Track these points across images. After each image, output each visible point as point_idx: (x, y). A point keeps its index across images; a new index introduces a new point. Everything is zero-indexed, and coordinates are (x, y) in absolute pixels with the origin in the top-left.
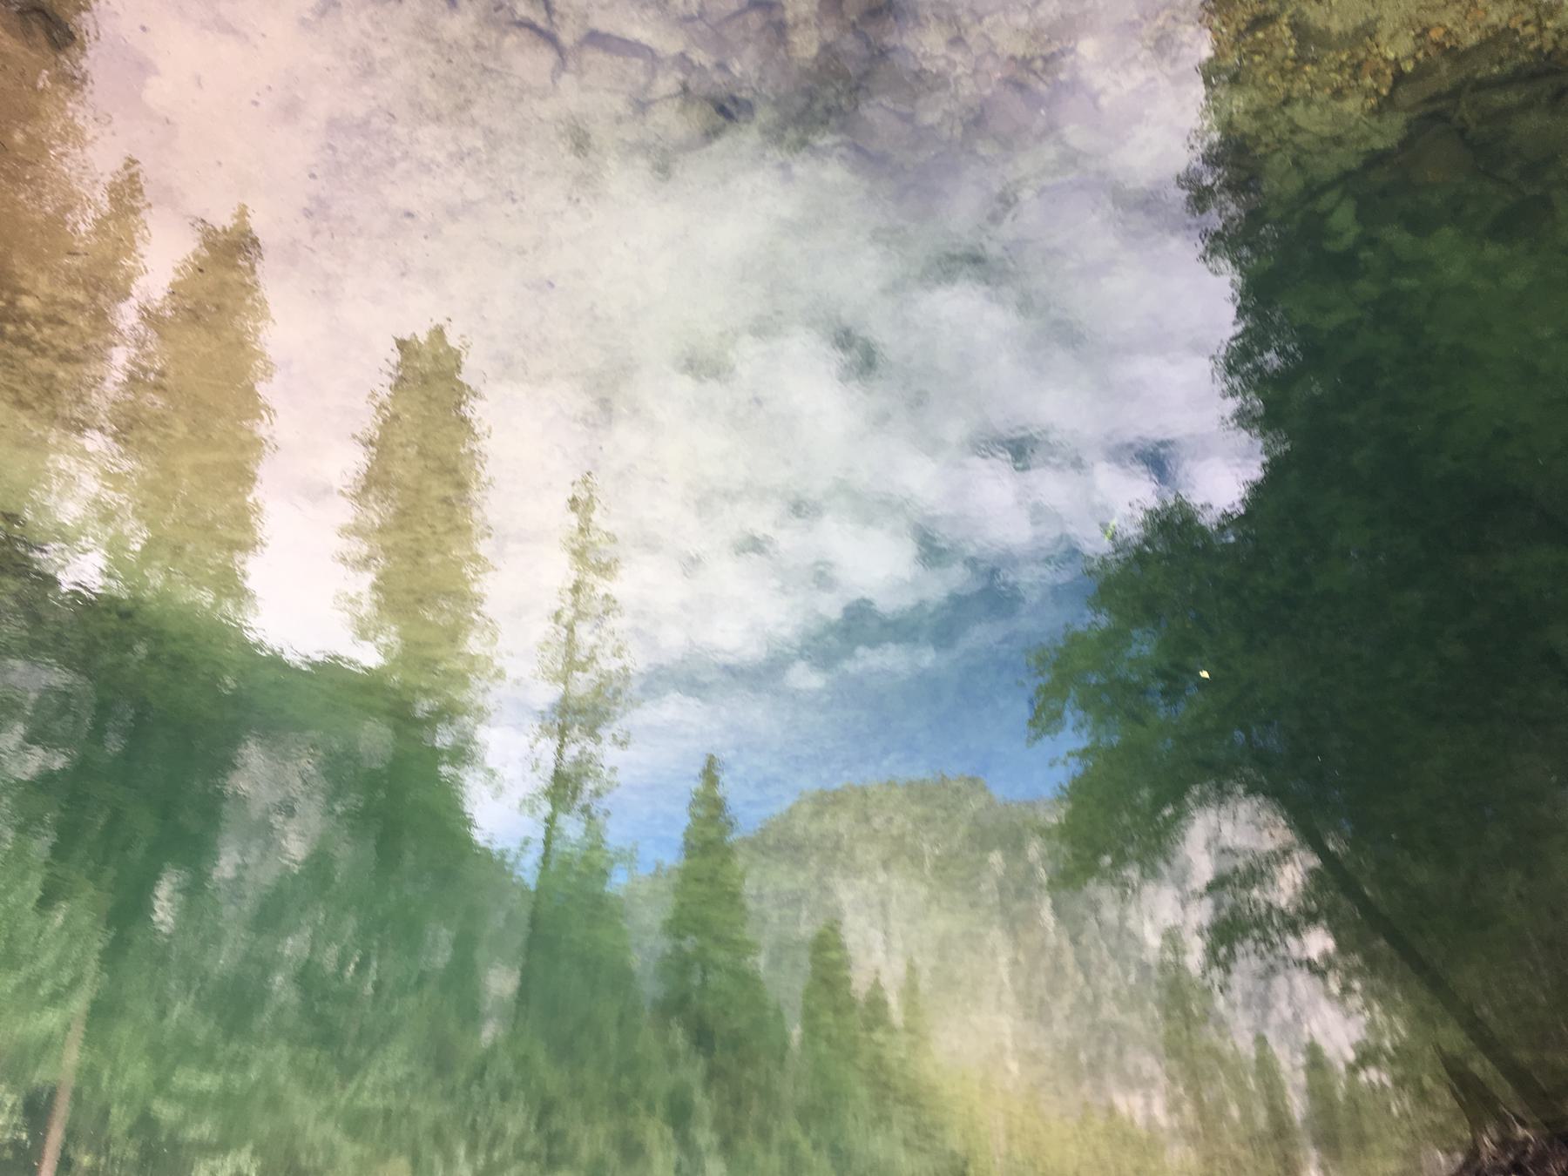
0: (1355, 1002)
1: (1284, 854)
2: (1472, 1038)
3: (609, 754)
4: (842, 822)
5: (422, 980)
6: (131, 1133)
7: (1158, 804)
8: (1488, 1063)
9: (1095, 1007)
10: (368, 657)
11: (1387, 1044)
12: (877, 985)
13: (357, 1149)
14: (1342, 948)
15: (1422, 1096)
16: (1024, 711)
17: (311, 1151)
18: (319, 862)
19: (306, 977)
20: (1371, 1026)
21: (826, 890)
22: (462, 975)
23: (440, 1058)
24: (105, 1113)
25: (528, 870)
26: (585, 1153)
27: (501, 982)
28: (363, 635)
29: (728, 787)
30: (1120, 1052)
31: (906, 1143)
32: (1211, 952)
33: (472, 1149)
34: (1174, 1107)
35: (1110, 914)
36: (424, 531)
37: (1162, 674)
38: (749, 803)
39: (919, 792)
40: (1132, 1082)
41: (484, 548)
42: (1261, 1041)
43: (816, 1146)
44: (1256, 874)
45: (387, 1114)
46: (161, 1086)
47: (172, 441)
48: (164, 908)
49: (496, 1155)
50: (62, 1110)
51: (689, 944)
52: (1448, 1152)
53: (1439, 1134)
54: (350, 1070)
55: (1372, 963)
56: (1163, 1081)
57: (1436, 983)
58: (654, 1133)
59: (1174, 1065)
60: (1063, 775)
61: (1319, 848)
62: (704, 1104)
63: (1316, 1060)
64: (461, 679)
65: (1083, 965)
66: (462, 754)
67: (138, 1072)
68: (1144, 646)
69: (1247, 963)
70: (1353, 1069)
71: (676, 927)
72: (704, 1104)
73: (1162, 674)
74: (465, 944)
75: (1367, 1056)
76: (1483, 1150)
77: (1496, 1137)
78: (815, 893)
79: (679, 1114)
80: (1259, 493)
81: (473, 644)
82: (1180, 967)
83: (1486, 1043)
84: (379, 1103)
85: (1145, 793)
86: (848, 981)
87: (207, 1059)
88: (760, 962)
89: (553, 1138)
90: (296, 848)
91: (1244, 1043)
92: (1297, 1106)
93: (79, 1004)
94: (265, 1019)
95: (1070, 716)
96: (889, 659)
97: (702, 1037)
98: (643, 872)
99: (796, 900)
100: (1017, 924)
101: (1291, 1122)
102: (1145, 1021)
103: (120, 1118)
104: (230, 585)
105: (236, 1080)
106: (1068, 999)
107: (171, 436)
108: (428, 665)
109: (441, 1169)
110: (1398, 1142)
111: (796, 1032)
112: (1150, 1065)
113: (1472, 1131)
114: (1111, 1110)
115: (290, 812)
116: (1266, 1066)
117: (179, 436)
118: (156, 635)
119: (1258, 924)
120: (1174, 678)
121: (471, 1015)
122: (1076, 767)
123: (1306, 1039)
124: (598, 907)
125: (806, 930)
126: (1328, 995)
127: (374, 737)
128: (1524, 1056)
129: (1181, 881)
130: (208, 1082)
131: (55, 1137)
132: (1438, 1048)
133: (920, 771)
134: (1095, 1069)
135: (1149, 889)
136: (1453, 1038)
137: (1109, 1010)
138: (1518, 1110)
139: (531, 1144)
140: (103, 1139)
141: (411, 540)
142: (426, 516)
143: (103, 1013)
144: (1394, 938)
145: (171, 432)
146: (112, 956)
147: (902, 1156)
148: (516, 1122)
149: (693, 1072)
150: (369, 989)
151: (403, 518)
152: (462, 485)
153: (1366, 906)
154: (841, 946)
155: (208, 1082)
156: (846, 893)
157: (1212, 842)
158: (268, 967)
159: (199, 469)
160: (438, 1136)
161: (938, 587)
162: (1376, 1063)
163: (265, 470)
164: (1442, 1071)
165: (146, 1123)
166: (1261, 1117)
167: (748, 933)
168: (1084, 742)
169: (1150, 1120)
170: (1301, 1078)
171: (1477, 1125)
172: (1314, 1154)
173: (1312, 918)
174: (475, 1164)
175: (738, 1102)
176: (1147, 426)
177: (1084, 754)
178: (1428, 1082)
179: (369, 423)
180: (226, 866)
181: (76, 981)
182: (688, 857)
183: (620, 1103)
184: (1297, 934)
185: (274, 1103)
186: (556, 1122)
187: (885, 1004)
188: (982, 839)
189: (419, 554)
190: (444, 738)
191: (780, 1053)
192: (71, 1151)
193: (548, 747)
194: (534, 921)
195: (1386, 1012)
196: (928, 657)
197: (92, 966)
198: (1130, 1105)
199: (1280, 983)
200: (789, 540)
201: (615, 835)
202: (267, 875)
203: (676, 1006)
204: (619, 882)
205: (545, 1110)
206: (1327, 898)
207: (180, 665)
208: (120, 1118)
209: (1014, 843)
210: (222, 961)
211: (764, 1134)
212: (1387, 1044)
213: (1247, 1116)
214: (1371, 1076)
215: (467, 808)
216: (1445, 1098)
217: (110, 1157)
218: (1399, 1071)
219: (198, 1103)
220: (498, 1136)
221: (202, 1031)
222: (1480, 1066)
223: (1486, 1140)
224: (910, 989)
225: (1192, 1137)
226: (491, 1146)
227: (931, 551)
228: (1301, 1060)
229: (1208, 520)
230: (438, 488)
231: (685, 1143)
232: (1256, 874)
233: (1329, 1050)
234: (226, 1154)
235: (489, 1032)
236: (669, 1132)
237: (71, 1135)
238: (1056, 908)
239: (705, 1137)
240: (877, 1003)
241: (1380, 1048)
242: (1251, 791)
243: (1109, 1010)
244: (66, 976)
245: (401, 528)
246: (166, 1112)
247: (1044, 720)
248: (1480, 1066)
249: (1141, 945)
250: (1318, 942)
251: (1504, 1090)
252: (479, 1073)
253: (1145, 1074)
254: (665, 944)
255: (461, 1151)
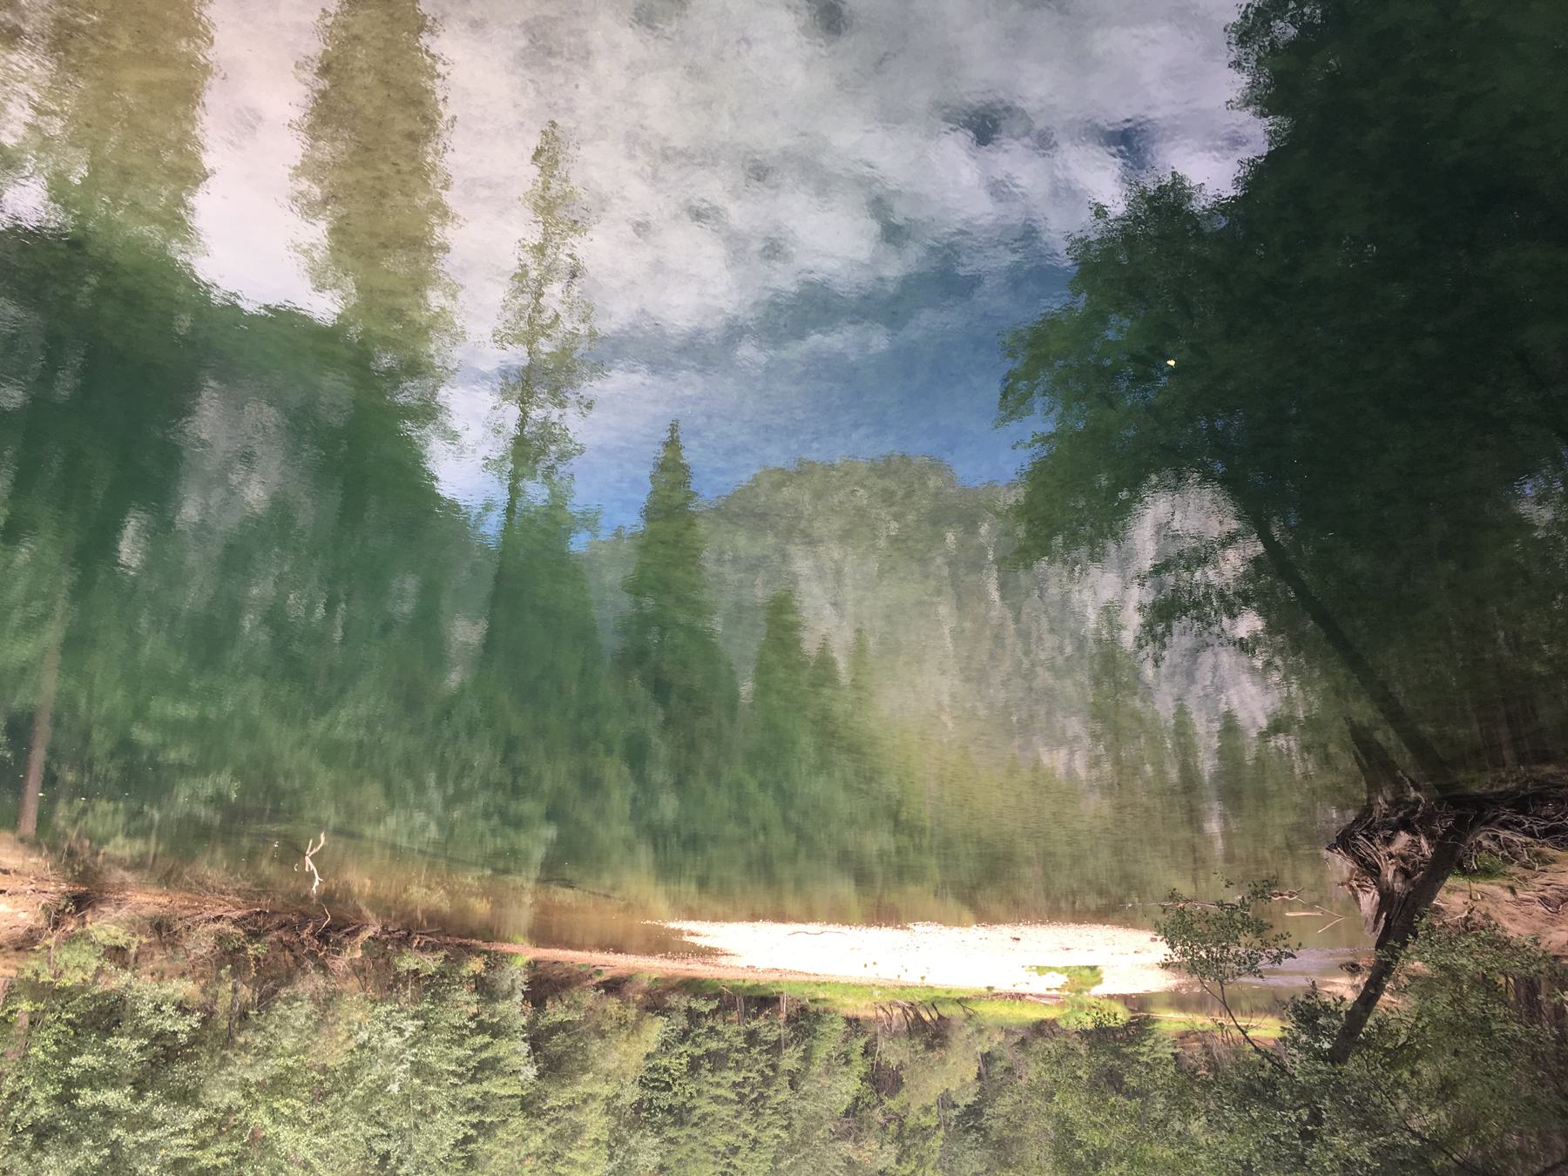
0: (1276, 677)
1: (1230, 540)
2: (1382, 711)
3: (572, 422)
4: (797, 495)
5: (387, 628)
6: (112, 755)
7: (1116, 489)
8: (1392, 733)
9: (1029, 675)
10: (324, 307)
11: (1301, 714)
12: (824, 648)
13: (331, 776)
14: (1271, 629)
15: (1327, 761)
16: (996, 390)
17: (288, 775)
18: (281, 508)
19: (274, 618)
20: (1288, 700)
21: (785, 557)
22: (427, 624)
23: (411, 698)
24: (86, 737)
25: (492, 525)
26: (546, 786)
27: (465, 632)
28: (320, 288)
29: (691, 454)
30: (1049, 713)
31: (847, 787)
32: (1148, 627)
33: (441, 780)
34: (1095, 763)
35: (1054, 591)
36: (386, 169)
37: (1135, 358)
38: (717, 471)
39: (884, 468)
40: (1058, 740)
41: (450, 198)
42: (1181, 711)
43: (763, 786)
44: (1201, 557)
45: (360, 744)
46: (139, 713)
47: (116, 53)
48: (130, 550)
49: (466, 784)
50: (43, 734)
51: (649, 602)
52: (1342, 809)
53: (1337, 794)
54: (323, 707)
55: (1297, 645)
56: (1087, 741)
57: (1354, 660)
58: (613, 770)
59: (1098, 727)
60: (1024, 458)
61: (1266, 538)
62: (661, 748)
63: (1230, 727)
64: (422, 332)
65: (1024, 635)
66: (428, 412)
67: (116, 699)
68: (1119, 329)
69: (1182, 637)
70: (1264, 736)
71: (636, 588)
72: (661, 748)
73: (1135, 358)
74: (430, 594)
75: (1278, 726)
76: (1377, 808)
77: (1389, 798)
78: (776, 558)
79: (636, 755)
80: (1259, 177)
81: (436, 299)
82: (1114, 641)
83: (1395, 715)
84: (353, 736)
85: (1103, 481)
86: (798, 641)
87: (181, 691)
88: (717, 624)
89: (516, 771)
90: (255, 495)
91: (1164, 707)
92: (1207, 765)
93: (53, 634)
94: (235, 656)
95: (1039, 402)
96: (835, 341)
97: (661, 689)
98: (605, 535)
99: (754, 566)
100: (964, 598)
101: (1199, 776)
102: (1077, 687)
103: (101, 741)
104: (176, 223)
105: (212, 712)
106: (1007, 666)
107: (114, 48)
108: (396, 314)
109: (412, 795)
110: (1297, 798)
111: (746, 688)
112: (1075, 726)
113: (1369, 792)
114: (1036, 766)
115: (247, 458)
116: (1182, 728)
117: (122, 47)
118: (106, 268)
119: (1197, 605)
120: (1145, 364)
121: (437, 658)
122: (1040, 451)
123: (1223, 707)
124: (563, 568)
125: (761, 593)
126: (1253, 669)
127: (334, 386)
128: (1428, 730)
129: (1126, 560)
130: (184, 711)
131: (38, 756)
132: (1348, 720)
133: (889, 446)
134: (1026, 728)
135: (1094, 570)
136: (1363, 710)
137: (1044, 678)
138: (1412, 774)
139: (496, 775)
140: (86, 758)
141: (375, 178)
142: (389, 153)
143: (76, 644)
144: (1323, 619)
145: (113, 43)
146: (80, 592)
147: (841, 796)
148: (483, 757)
149: (651, 722)
150: (338, 635)
151: (365, 153)
152: (430, 121)
153: (1301, 591)
154: (794, 611)
155: (184, 711)
156: (802, 564)
157: (1163, 531)
158: (236, 610)
159: (145, 88)
160: (409, 764)
161: (894, 268)
162: (1287, 732)
163: (213, 96)
164: (1348, 739)
165: (126, 746)
166: (1173, 775)
167: (706, 596)
168: (1050, 427)
169: (1070, 772)
170: (1215, 743)
171: (1373, 787)
172: (1217, 806)
173: (1246, 599)
174: (445, 792)
175: (692, 746)
176: (1119, 112)
177: (1046, 439)
178: (1333, 749)
179: (315, 47)
180: (190, 511)
181: (45, 617)
182: (649, 520)
183: (580, 744)
184: (1233, 616)
185: (251, 732)
186: (521, 758)
187: (833, 662)
188: (938, 518)
189: (383, 194)
190: (406, 396)
191: (732, 704)
192: (54, 767)
193: (512, 412)
194: (499, 578)
195: (1301, 687)
196: (879, 341)
197: (61, 605)
198: (1055, 760)
199: (1207, 658)
200: (740, 214)
201: (582, 497)
202: (229, 523)
203: (634, 658)
204: (579, 544)
205: (510, 747)
206: (1266, 580)
207: (133, 301)
208: (101, 741)
209: (969, 522)
210: (193, 598)
211: (714, 775)
212: (1301, 714)
213: (1161, 772)
214: (1281, 741)
215: (430, 466)
216: (1347, 762)
217: (93, 775)
218: (1308, 737)
219: (177, 729)
220: (466, 767)
221: (177, 664)
222: (1386, 736)
223: (1380, 800)
224: (859, 652)
225: (1108, 790)
226: (459, 778)
227: (893, 234)
228: (1217, 726)
229: (1199, 204)
230: (402, 122)
231: (641, 778)
232: (1201, 557)
233: (1242, 717)
234: (207, 776)
235: (454, 679)
236: (625, 769)
237: (53, 752)
238: (1002, 586)
239: (659, 775)
240: (825, 663)
241: (1291, 718)
242: (1207, 477)
243: (1044, 678)
244: (37, 606)
245: (363, 164)
246: (144, 736)
247: (1013, 401)
248: (1386, 736)
249: (1081, 619)
250: (1249, 624)
251: (1404, 758)
252: (447, 713)
253: (1070, 734)
254: (625, 602)
255: (431, 779)
